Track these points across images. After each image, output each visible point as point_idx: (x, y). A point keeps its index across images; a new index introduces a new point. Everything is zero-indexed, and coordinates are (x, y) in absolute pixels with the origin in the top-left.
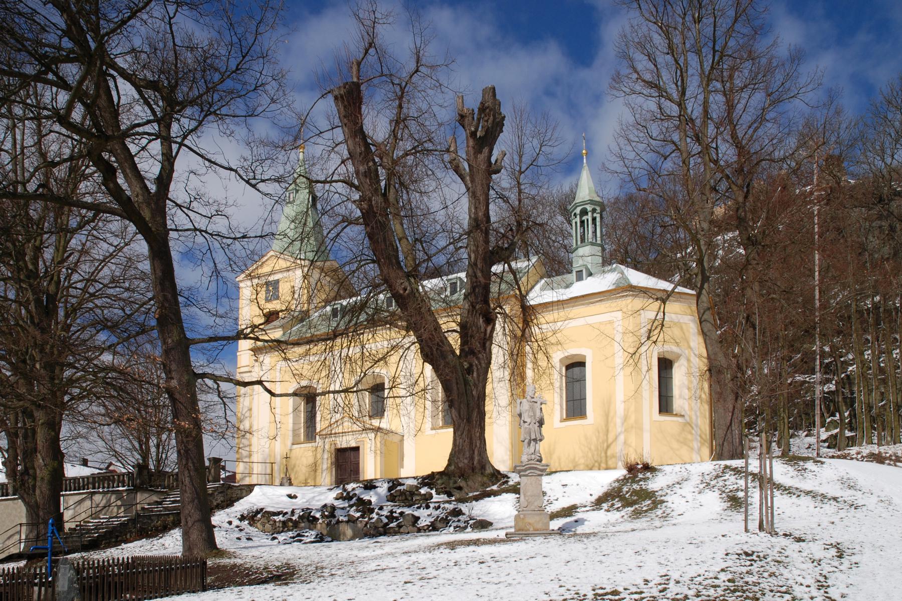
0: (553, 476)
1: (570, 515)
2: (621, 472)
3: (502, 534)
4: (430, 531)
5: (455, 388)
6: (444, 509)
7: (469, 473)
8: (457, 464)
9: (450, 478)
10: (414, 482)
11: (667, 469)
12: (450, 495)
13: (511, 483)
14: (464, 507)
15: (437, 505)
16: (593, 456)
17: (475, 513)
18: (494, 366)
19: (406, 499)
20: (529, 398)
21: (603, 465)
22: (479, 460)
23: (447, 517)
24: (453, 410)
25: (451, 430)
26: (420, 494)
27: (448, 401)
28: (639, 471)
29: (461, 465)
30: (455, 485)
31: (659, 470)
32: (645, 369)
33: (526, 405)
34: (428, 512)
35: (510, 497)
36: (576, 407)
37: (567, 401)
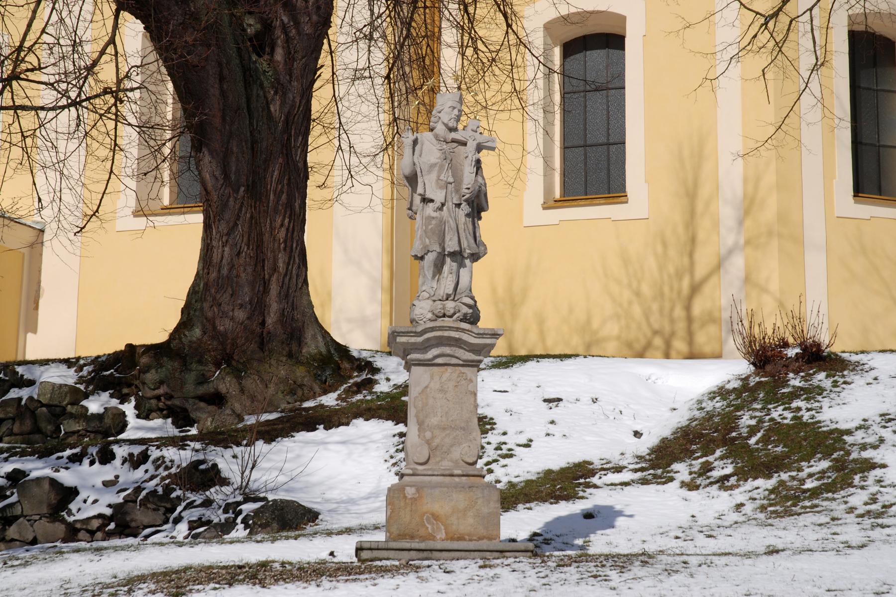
0: (518, 371)
1: (570, 496)
2: (734, 368)
3: (345, 550)
4: (109, 535)
5: (214, 91)
6: (159, 462)
7: (247, 351)
8: (212, 321)
9: (185, 366)
10: (66, 377)
11: (880, 363)
12: (182, 419)
13: (382, 387)
14: (226, 461)
15: (137, 450)
16: (647, 315)
17: (260, 478)
18: (339, 32)
19: (37, 430)
20: (440, 129)
21: (679, 345)
22: (282, 313)
23: (168, 490)
24: (207, 158)
25: (197, 219)
26: (84, 414)
27: (189, 127)
28: (789, 365)
29: (224, 325)
30: (202, 390)
31: (856, 367)
32: (806, 61)
33: (431, 151)
34: (107, 472)
35: (380, 431)
36: (592, 167)
37: (565, 148)
